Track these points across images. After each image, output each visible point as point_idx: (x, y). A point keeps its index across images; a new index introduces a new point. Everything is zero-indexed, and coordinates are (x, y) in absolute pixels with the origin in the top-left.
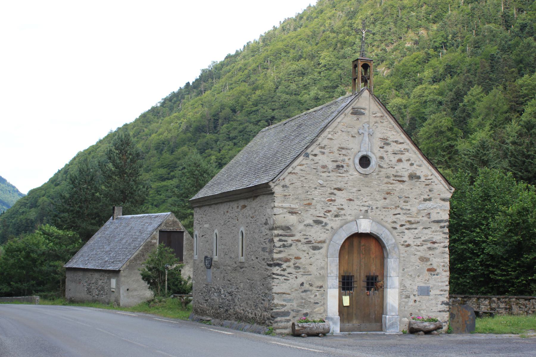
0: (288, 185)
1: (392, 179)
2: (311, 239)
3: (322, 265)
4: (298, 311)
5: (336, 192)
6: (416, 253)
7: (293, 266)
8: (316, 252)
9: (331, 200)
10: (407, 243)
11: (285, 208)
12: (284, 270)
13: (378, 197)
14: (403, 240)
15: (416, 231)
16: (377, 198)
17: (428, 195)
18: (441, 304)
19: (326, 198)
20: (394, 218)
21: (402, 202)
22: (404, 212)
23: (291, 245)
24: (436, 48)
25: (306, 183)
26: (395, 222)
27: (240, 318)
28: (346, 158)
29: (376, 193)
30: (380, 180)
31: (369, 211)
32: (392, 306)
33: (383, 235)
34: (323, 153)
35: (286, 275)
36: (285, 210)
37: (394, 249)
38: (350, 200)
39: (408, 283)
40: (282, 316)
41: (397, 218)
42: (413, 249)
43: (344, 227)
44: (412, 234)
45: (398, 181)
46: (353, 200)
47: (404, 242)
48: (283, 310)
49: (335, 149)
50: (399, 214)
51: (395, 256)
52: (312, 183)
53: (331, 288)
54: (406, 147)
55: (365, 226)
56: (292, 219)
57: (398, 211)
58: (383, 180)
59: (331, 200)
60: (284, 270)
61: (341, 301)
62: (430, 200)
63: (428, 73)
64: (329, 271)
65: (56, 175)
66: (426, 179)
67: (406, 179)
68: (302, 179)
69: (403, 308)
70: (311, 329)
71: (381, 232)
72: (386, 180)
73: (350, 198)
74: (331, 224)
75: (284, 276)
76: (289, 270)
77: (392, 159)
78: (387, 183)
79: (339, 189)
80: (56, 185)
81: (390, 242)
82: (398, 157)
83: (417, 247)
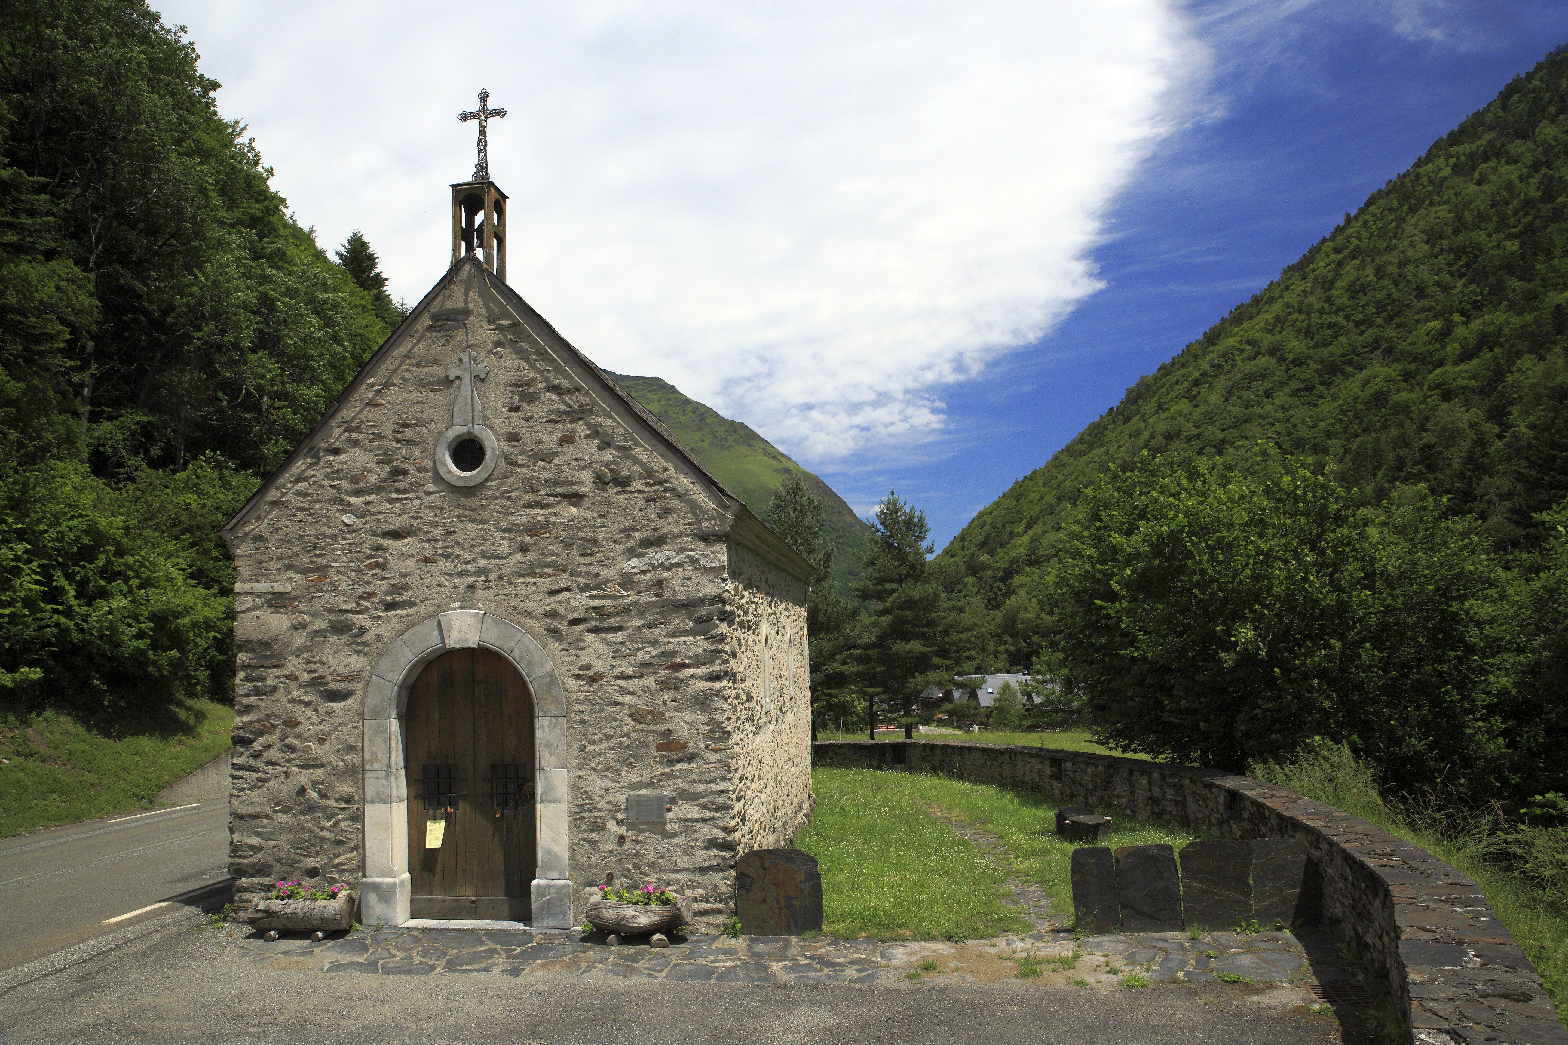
0: (267, 535)
1: (542, 492)
2: (321, 671)
3: (351, 740)
4: (293, 864)
5: (385, 542)
6: (621, 699)
7: (278, 745)
8: (337, 706)
9: (377, 565)
10: (590, 673)
11: (259, 595)
12: (257, 756)
13: (504, 545)
14: (580, 662)
15: (619, 636)
16: (501, 550)
17: (656, 530)
18: (707, 848)
19: (361, 561)
20: (551, 603)
21: (575, 553)
22: (582, 581)
23: (274, 689)
24: (1463, 313)
25: (312, 524)
26: (553, 614)
27: (1039, 756)
28: (417, 451)
29: (497, 535)
30: (509, 498)
31: (479, 585)
32: (549, 852)
33: (517, 653)
34: (355, 443)
35: (263, 767)
36: (259, 601)
37: (549, 691)
38: (427, 560)
39: (596, 784)
40: (252, 876)
41: (560, 602)
42: (610, 689)
43: (406, 636)
44: (608, 644)
45: (562, 495)
46: (435, 561)
47: (581, 668)
48: (254, 860)
49: (387, 429)
50: (568, 589)
51: (553, 709)
52: (326, 524)
53: (372, 802)
54: (584, 400)
55: (464, 628)
56: (277, 622)
57: (564, 580)
58: (519, 497)
59: (377, 565)
60: (257, 756)
61: (416, 834)
62: (659, 541)
63: (1453, 349)
64: (367, 756)
65: (952, 543)
66: (648, 484)
67: (587, 488)
68: (301, 516)
69: (585, 859)
70: (293, 916)
71: (512, 644)
72: (528, 497)
73: (427, 553)
74: (374, 629)
75: (256, 770)
76: (269, 755)
77: (544, 436)
78: (529, 506)
79: (396, 535)
80: (952, 556)
81: (538, 672)
82: (565, 427)
83: (623, 683)
